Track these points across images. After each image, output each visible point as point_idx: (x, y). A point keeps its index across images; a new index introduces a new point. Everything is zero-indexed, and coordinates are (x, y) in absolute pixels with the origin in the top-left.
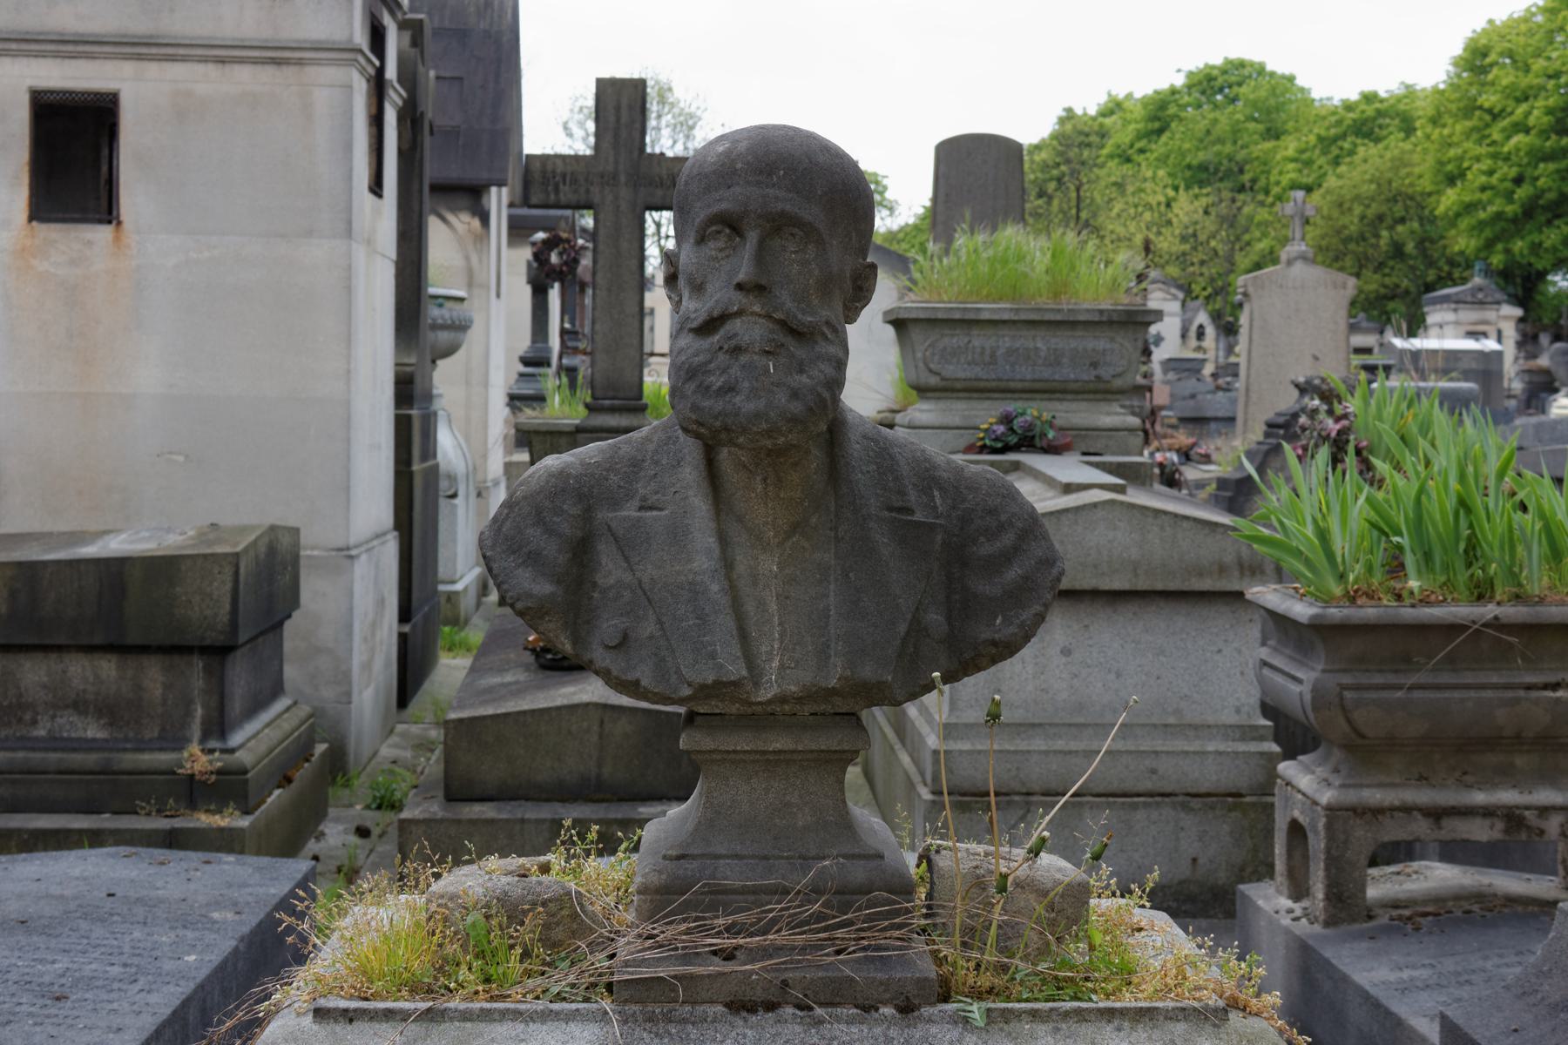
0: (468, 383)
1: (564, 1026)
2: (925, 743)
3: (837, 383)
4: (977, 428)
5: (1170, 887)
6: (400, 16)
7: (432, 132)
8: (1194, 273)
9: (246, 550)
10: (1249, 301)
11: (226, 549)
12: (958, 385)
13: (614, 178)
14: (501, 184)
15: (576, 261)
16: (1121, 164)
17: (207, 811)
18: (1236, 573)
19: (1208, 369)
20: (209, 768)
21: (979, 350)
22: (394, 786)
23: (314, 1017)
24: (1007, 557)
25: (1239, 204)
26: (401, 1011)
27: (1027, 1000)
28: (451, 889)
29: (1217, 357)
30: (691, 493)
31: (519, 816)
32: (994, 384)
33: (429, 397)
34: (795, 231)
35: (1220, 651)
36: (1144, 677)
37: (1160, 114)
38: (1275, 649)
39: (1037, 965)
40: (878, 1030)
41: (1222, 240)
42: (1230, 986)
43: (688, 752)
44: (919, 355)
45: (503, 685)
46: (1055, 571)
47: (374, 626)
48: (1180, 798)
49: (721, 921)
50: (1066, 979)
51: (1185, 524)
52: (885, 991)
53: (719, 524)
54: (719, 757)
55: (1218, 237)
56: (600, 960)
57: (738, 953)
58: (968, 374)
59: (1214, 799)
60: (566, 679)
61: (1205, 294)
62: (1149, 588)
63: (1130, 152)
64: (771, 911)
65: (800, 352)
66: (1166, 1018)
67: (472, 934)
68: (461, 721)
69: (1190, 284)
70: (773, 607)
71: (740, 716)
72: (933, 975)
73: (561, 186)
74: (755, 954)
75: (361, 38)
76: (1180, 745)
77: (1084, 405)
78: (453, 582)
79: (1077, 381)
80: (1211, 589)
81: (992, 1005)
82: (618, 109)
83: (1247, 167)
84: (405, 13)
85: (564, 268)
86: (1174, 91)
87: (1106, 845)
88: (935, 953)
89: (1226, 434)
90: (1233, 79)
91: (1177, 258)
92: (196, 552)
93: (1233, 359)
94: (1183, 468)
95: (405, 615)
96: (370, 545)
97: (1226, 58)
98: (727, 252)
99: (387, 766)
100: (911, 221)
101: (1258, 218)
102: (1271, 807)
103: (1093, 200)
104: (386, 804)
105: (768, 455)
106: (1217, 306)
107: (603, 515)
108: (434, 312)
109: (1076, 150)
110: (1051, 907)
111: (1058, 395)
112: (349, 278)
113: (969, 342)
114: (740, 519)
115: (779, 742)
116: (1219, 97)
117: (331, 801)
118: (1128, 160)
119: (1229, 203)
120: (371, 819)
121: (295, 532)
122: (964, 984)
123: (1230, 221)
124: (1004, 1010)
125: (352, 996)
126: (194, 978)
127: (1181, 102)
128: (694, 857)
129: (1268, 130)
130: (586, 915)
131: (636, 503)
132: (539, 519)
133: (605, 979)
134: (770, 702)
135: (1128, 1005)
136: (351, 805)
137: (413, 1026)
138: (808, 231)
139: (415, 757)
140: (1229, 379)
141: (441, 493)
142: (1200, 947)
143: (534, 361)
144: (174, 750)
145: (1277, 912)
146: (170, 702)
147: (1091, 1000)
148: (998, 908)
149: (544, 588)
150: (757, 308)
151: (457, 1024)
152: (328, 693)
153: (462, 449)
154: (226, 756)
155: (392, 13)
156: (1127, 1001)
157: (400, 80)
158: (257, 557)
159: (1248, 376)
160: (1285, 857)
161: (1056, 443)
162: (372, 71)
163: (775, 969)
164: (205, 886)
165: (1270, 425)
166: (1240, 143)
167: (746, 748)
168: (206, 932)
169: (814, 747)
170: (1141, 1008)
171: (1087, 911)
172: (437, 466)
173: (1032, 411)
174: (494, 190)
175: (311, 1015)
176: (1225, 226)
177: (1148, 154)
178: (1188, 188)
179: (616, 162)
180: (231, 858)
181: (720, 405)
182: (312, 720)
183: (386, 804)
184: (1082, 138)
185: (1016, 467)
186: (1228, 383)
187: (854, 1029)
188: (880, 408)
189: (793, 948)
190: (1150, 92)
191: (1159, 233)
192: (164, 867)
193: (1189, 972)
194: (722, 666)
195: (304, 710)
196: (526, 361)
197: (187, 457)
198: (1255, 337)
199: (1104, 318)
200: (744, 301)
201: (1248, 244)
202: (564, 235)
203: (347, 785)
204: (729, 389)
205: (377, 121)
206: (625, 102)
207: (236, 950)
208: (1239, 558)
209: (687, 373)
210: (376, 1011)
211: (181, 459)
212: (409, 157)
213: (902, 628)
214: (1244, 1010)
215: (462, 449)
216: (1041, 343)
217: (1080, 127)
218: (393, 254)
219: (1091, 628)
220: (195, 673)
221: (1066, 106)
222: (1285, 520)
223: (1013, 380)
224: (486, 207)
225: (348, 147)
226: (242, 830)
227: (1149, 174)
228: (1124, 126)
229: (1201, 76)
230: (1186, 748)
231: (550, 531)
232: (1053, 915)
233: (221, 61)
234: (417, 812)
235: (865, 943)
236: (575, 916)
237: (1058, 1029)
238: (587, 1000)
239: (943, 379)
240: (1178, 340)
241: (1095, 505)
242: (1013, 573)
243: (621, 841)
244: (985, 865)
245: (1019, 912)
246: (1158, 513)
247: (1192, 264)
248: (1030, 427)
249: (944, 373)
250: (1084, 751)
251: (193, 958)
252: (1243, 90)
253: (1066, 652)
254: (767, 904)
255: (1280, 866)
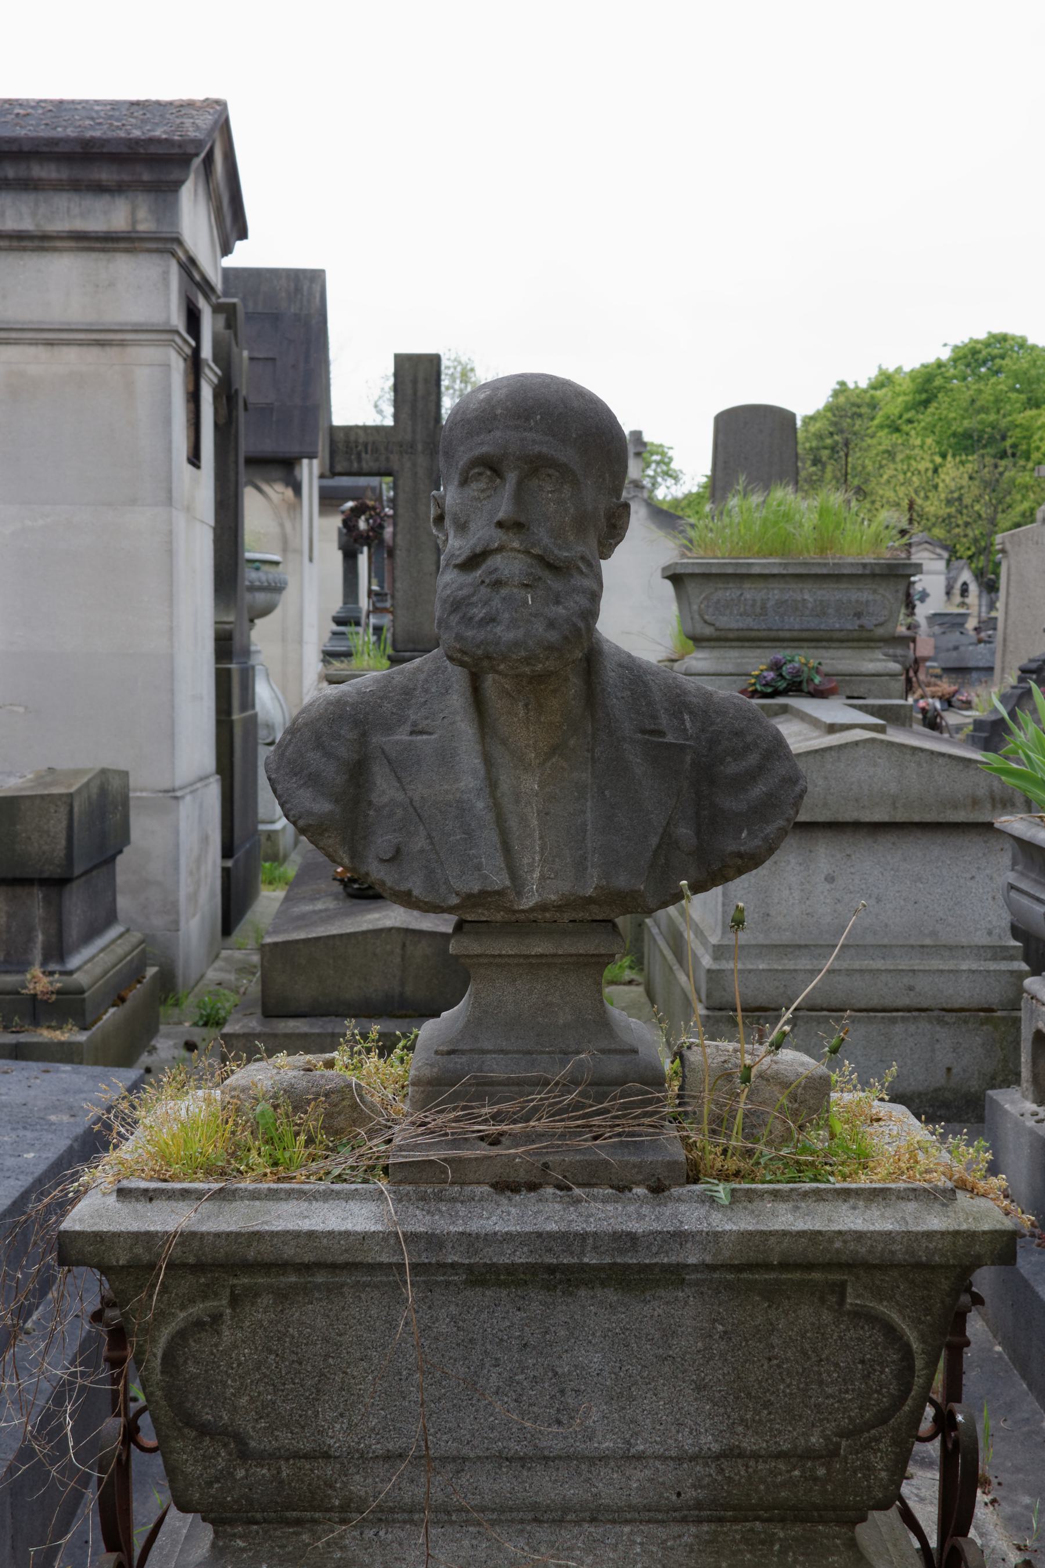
0: (284, 640)
1: (344, 1204)
2: (700, 963)
3: (591, 614)
4: (750, 675)
5: (926, 1094)
6: (214, 299)
7: (246, 409)
8: (958, 535)
9: (79, 791)
10: (1006, 557)
11: (63, 790)
12: (731, 635)
13: (412, 447)
14: (311, 456)
15: (381, 527)
16: (891, 433)
17: (49, 1027)
18: (989, 806)
19: (971, 624)
20: (50, 989)
21: (750, 602)
22: (219, 1005)
23: (118, 1196)
24: (752, 776)
25: (1001, 469)
26: (196, 1191)
27: (770, 1182)
28: (243, 1082)
29: (980, 613)
30: (458, 718)
31: (330, 1030)
32: (764, 634)
33: (247, 653)
34: (551, 471)
35: (973, 878)
36: (902, 903)
37: (927, 386)
38: (1022, 874)
39: (780, 1150)
40: (631, 1209)
41: (986, 504)
42: (958, 1169)
43: (457, 957)
44: (695, 607)
45: (315, 912)
46: (798, 789)
47: (199, 861)
48: (935, 1013)
49: (486, 1110)
50: (807, 1163)
51: (941, 761)
52: (637, 1173)
53: (484, 746)
54: (486, 961)
55: (982, 501)
56: (377, 1145)
57: (503, 1139)
58: (741, 625)
59: (967, 1014)
60: (372, 906)
61: (970, 553)
62: (907, 820)
63: (900, 422)
64: (532, 1100)
65: (556, 584)
66: (898, 1198)
67: (261, 1122)
68: (276, 944)
69: (955, 547)
70: (535, 822)
71: (505, 924)
72: (683, 1158)
73: (363, 455)
74: (517, 1140)
75: (178, 320)
76: (936, 964)
77: (848, 653)
78: (273, 822)
79: (842, 630)
80: (965, 820)
81: (738, 1186)
82: (415, 382)
83: (1009, 434)
84: (219, 297)
85: (371, 534)
86: (940, 365)
87: (843, 1040)
88: (684, 1139)
89: (986, 682)
90: (996, 352)
91: (944, 521)
92: (34, 793)
93: (993, 614)
94: (944, 714)
95: (228, 851)
96: (195, 787)
97: (989, 333)
98: (488, 493)
99: (213, 988)
100: (695, 490)
101: (1019, 481)
102: (1017, 1021)
103: (864, 467)
104: (211, 1021)
105: (530, 683)
106: (980, 565)
107: (377, 739)
108: (250, 576)
109: (849, 420)
110: (793, 1098)
111: (824, 644)
112: (170, 543)
113: (741, 595)
114: (504, 742)
115: (540, 947)
116: (983, 370)
117: (162, 1019)
118: (898, 430)
119: (991, 468)
120: (198, 1034)
121: (125, 774)
122: (712, 1167)
123: (991, 485)
124: (748, 1190)
125: (152, 1177)
126: (32, 1173)
127: (947, 375)
128: (463, 1052)
129: (1029, 399)
130: (365, 1105)
131: (408, 728)
132: (319, 744)
133: (382, 1162)
134: (532, 910)
135: (862, 1186)
136: (180, 1023)
137: (207, 1205)
138: (564, 472)
139: (237, 979)
140: (990, 632)
141: (260, 741)
142: (933, 1134)
143: (346, 620)
144: (18, 972)
145: (1022, 1115)
146: (13, 930)
147: (828, 1181)
148: (744, 1096)
149: (324, 807)
150: (516, 544)
151: (247, 1202)
152: (158, 922)
153: (279, 701)
154: (64, 978)
155: (207, 297)
156: (863, 1182)
157: (215, 360)
158: (89, 797)
159: (1005, 628)
160: (1030, 1065)
161: (821, 688)
162: (188, 351)
163: (537, 1153)
164: (44, 1092)
165: (1025, 671)
166: (1002, 412)
167: (510, 952)
168: (44, 1133)
169: (573, 951)
170: (875, 1189)
171: (828, 1102)
172: (256, 715)
173: (800, 658)
174: (305, 462)
175: (115, 1194)
176: (988, 491)
177: (916, 424)
178: (954, 456)
179: (414, 432)
180: (68, 1068)
181: (481, 635)
182: (143, 946)
183: (211, 1021)
184: (855, 409)
185: (785, 709)
186: (990, 637)
187: (610, 1207)
188: (660, 659)
189: (554, 1135)
190: (917, 366)
191: (927, 498)
192: (7, 1076)
193: (921, 1156)
194: (486, 877)
195: (136, 936)
196: (339, 621)
197: (26, 708)
198: (1012, 590)
199: (868, 572)
200: (505, 538)
201: (1010, 506)
202: (371, 503)
203: (177, 1004)
204: (491, 620)
205: (194, 397)
206: (421, 376)
207: (71, 1147)
208: (992, 792)
209: (452, 606)
210: (173, 1191)
211: (21, 710)
212: (224, 430)
213: (654, 841)
214: (972, 1191)
215: (279, 701)
216: (809, 595)
217: (854, 399)
218: (211, 521)
219: (853, 857)
220: (36, 903)
221: (840, 379)
222: (1031, 754)
223: (782, 630)
224: (298, 478)
225: (168, 421)
226: (80, 1044)
227: (918, 442)
228: (893, 398)
229: (966, 350)
230: (941, 967)
231: (328, 754)
232: (796, 1105)
233: (50, 343)
234: (237, 1028)
235: (619, 1129)
236: (355, 1106)
237: (798, 1208)
238: (365, 1181)
239: (717, 630)
240: (943, 597)
241: (856, 743)
242: (758, 790)
243: (399, 1040)
244: (733, 1060)
245: (764, 1102)
246: (915, 750)
247: (958, 526)
248: (798, 673)
249: (718, 624)
250: (847, 970)
251: (32, 1155)
252: (1007, 361)
253: (830, 879)
254: (532, 1094)
255: (1025, 1072)
